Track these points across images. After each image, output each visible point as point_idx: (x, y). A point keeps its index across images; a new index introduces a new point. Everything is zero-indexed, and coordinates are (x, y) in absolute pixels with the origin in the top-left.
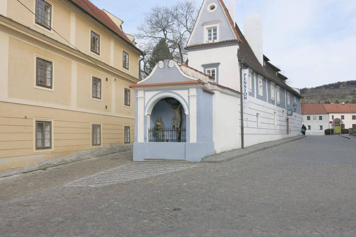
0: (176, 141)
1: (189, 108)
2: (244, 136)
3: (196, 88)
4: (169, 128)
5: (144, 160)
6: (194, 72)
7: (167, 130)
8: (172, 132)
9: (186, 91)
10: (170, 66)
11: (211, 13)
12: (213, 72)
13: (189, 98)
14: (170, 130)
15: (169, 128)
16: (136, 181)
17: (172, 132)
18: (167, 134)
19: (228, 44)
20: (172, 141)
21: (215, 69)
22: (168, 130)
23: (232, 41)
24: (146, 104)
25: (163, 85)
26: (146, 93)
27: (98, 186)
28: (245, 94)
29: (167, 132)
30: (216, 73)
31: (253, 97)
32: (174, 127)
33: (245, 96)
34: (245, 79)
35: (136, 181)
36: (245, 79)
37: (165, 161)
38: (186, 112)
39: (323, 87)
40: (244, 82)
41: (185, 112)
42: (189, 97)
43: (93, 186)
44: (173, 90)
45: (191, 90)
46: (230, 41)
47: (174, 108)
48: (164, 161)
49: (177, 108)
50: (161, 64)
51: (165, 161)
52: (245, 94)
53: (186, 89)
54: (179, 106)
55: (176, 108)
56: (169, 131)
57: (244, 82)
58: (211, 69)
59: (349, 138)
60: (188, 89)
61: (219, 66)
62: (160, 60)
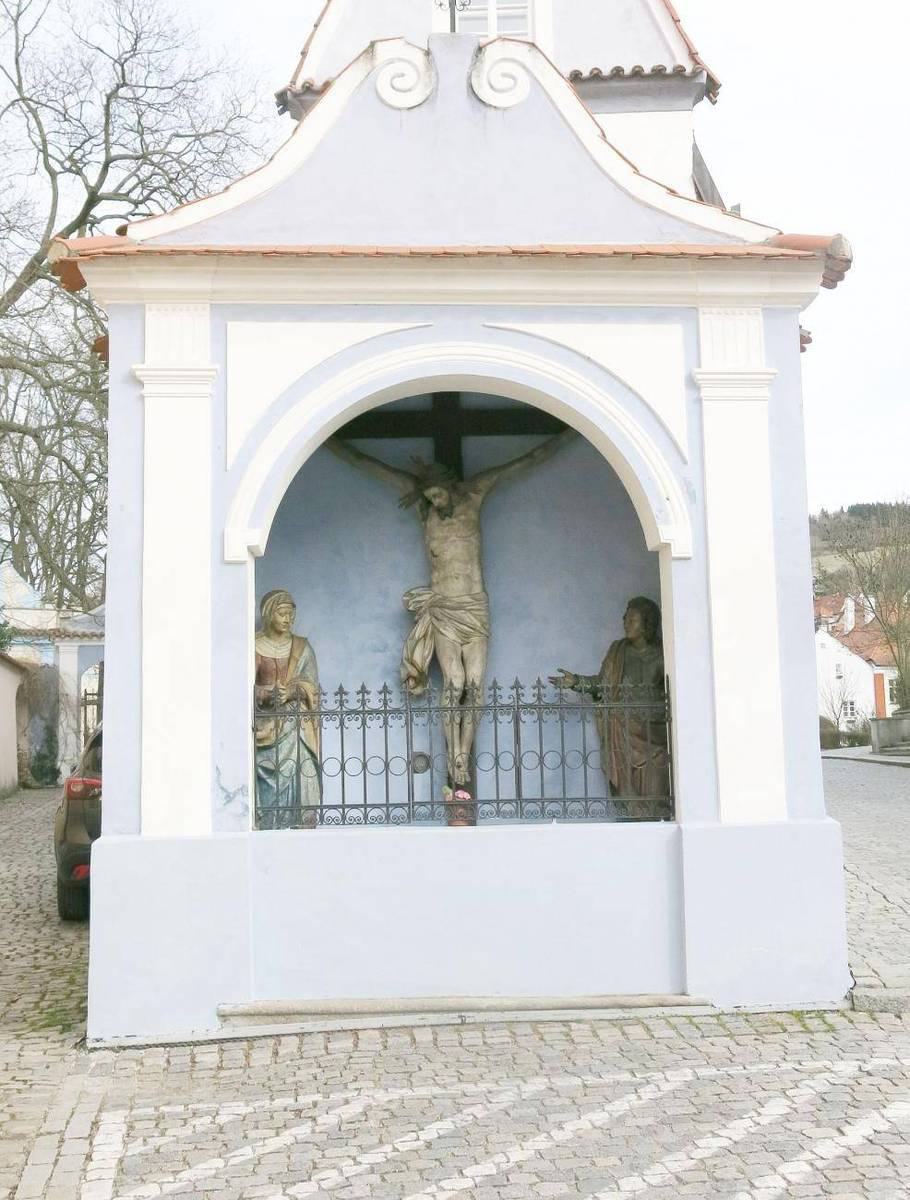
0: (553, 815)
1: (696, 496)
3: (769, 313)
4: (352, 688)
5: (217, 1022)
7: (353, 704)
8: (517, 720)
9: (668, 337)
13: (699, 401)
14: (385, 713)
15: (352, 688)
17: (517, 720)
18: (353, 750)
19: (624, 94)
20: (390, 814)
22: (363, 714)
23: (659, 73)
26: (237, 329)
29: (353, 725)
37: (471, 1017)
42: (692, 384)
44: (535, 313)
45: (710, 322)
46: (648, 77)
48: (454, 1018)
49: (458, 510)
50: (399, 67)
51: (471, 1017)
55: (445, 513)
56: (375, 724)
60: (688, 312)
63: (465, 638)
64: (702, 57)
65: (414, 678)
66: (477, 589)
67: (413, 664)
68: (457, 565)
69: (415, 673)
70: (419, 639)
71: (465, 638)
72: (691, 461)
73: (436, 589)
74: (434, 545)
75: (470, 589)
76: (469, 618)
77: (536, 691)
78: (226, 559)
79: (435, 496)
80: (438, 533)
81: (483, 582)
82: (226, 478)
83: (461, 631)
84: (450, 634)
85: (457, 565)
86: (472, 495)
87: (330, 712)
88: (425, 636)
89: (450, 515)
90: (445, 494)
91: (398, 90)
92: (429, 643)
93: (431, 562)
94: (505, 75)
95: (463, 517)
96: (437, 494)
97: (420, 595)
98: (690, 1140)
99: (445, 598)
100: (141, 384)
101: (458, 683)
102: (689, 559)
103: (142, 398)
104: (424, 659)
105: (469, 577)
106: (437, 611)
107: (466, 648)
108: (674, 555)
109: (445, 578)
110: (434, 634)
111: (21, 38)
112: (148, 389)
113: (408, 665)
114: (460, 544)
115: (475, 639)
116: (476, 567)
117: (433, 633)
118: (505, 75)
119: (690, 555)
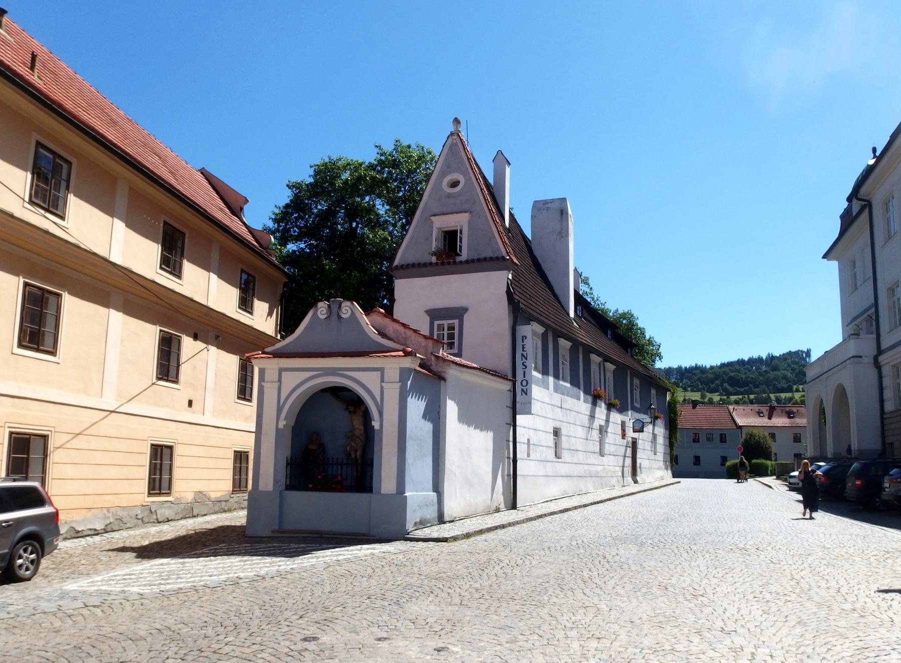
1: (381, 414)
2: (518, 445)
6: (401, 329)
10: (343, 316)
11: (450, 196)
12: (451, 328)
16: (240, 581)
21: (456, 322)
24: (379, 400)
25: (821, 438)
27: (146, 590)
28: (524, 383)
30: (456, 332)
31: (57, 520)
32: (350, 455)
33: (525, 388)
34: (523, 348)
35: (240, 581)
36: (523, 348)
38: (376, 424)
39: (363, 409)
40: (523, 355)
41: (373, 423)
43: (136, 589)
47: (350, 413)
52: (524, 383)
53: (45, 317)
54: (363, 409)
55: (355, 412)
57: (523, 355)
58: (446, 323)
59: (770, 487)
61: (465, 317)
62: (321, 301)
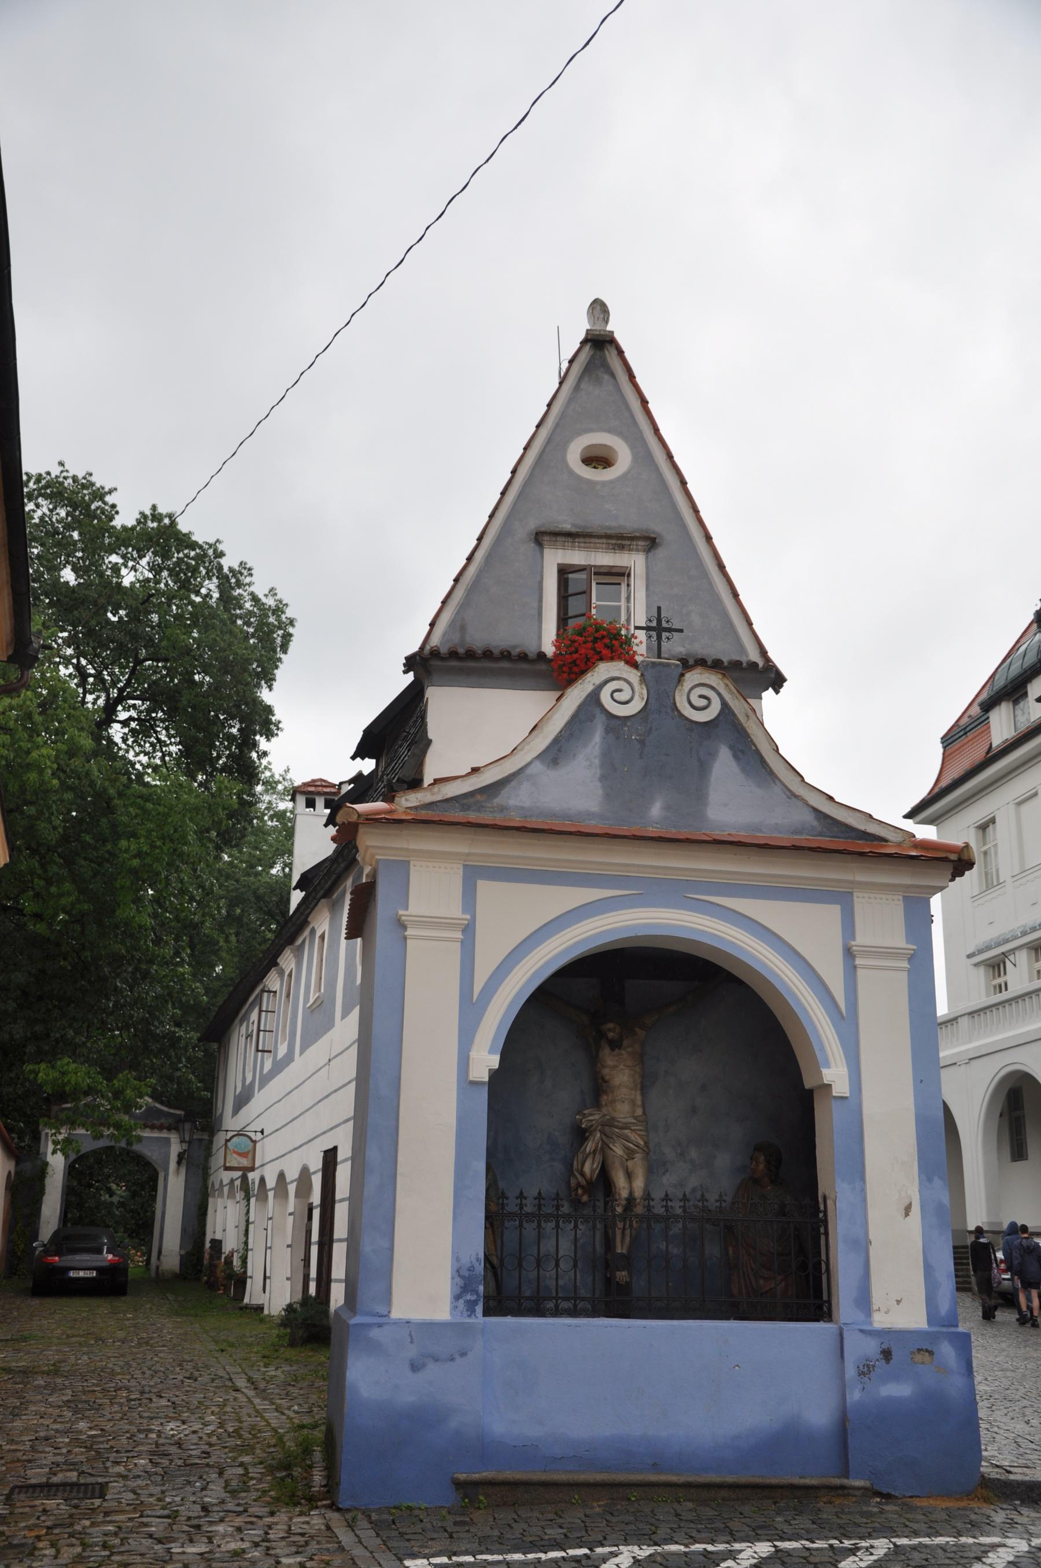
42: (849, 954)
49: (626, 1043)
63: (630, 1154)
64: (771, 654)
65: (582, 1187)
66: (639, 1112)
67: (583, 1174)
68: (624, 1090)
69: (583, 1182)
70: (590, 1153)
71: (630, 1154)
72: (847, 1021)
73: (604, 1110)
74: (606, 1071)
75: (634, 1112)
76: (633, 1136)
77: (682, 1204)
78: (471, 1078)
79: (610, 1030)
80: (610, 1061)
81: (644, 1106)
82: (471, 1010)
83: (628, 1148)
84: (618, 1150)
85: (624, 1090)
86: (637, 1030)
87: (549, 1214)
88: (595, 1151)
89: (619, 1047)
90: (618, 1029)
91: (615, 701)
92: (599, 1158)
93: (598, 1090)
94: (701, 696)
95: (629, 1049)
96: (611, 1029)
97: (591, 1115)
98: (960, 1534)
99: (613, 1119)
100: (404, 927)
101: (625, 1194)
102: (846, 1098)
103: (405, 938)
104: (593, 1171)
105: (633, 1102)
106: (607, 1129)
107: (630, 1163)
108: (834, 1094)
109: (613, 1101)
110: (604, 1149)
111: (840, 844)
112: (409, 932)
113: (578, 1176)
114: (627, 1072)
115: (638, 1156)
116: (639, 1092)
117: (602, 1148)
118: (701, 696)
119: (848, 1095)
